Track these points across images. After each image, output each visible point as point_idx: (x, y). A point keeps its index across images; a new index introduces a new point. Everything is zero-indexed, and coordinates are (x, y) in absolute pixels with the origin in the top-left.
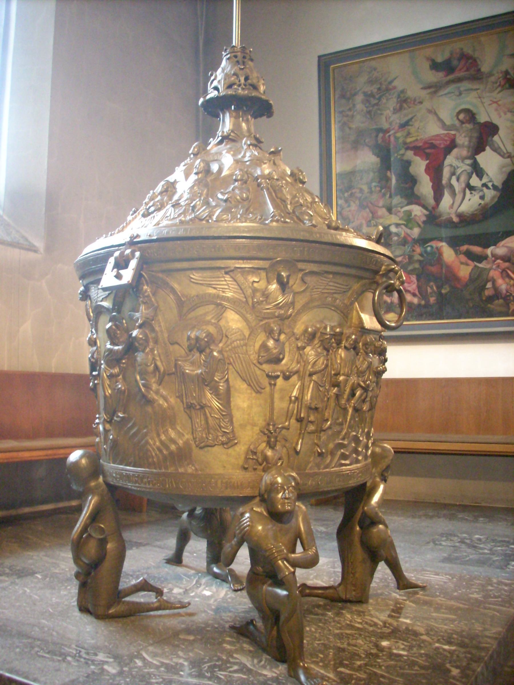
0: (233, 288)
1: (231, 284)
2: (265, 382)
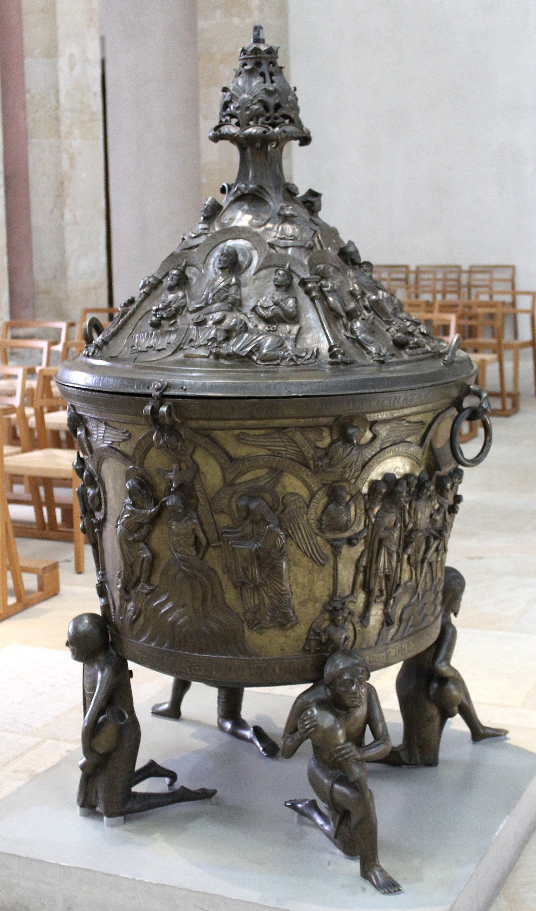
0: (291, 449)
1: (290, 446)
2: (327, 550)
